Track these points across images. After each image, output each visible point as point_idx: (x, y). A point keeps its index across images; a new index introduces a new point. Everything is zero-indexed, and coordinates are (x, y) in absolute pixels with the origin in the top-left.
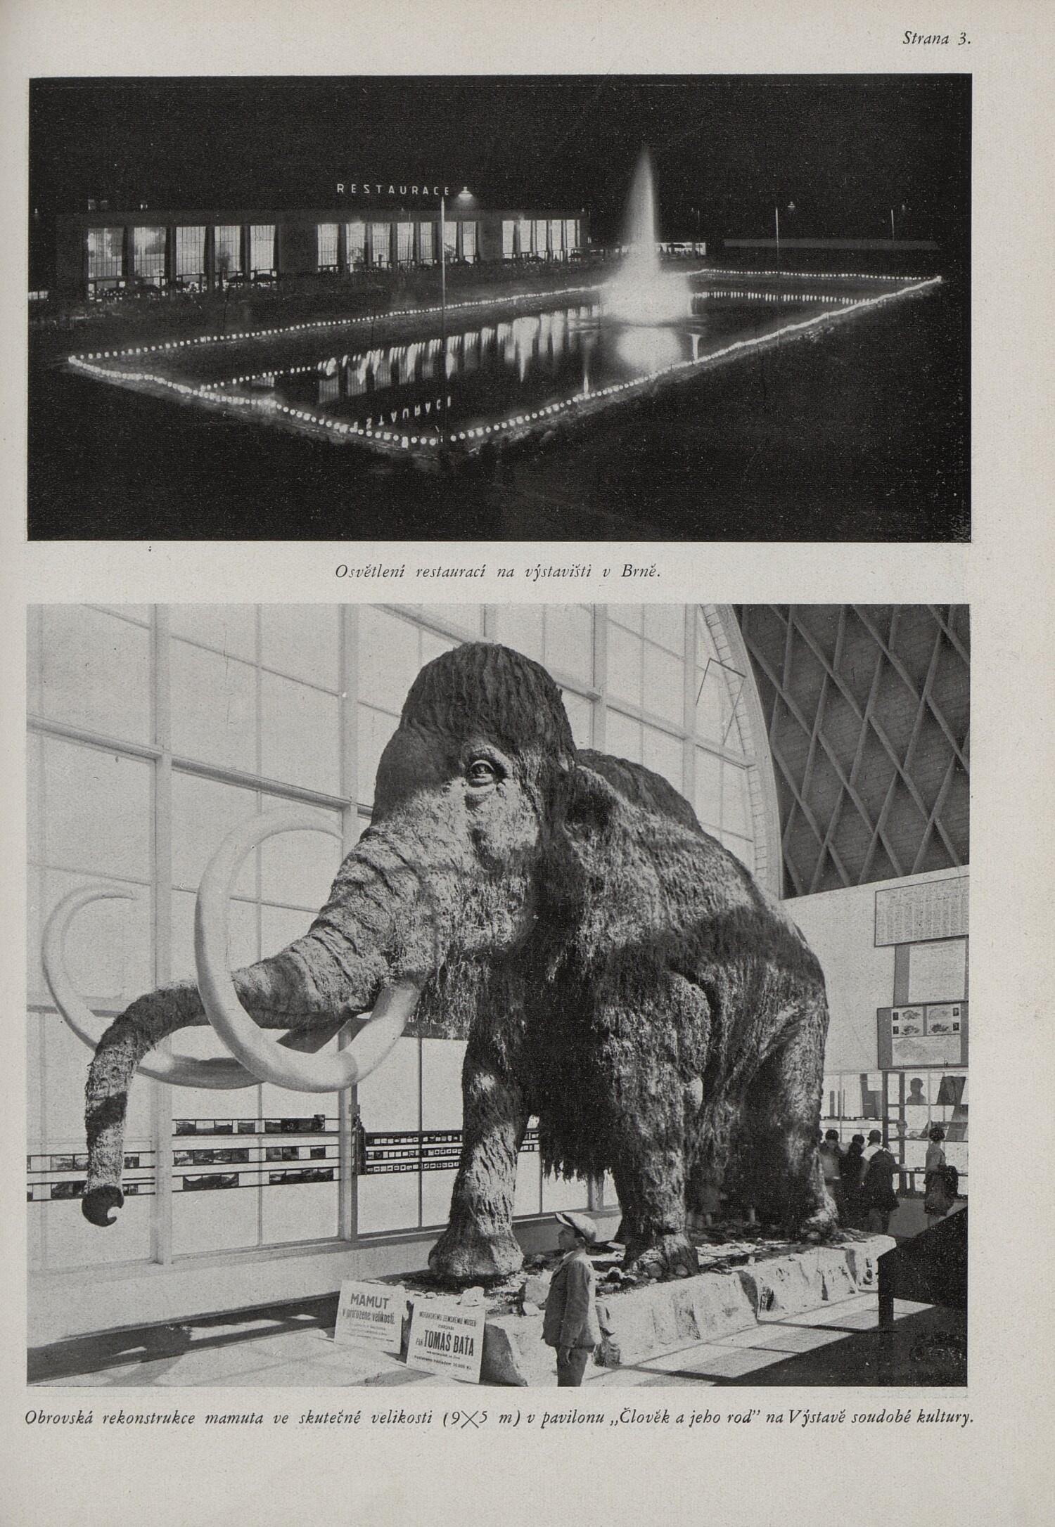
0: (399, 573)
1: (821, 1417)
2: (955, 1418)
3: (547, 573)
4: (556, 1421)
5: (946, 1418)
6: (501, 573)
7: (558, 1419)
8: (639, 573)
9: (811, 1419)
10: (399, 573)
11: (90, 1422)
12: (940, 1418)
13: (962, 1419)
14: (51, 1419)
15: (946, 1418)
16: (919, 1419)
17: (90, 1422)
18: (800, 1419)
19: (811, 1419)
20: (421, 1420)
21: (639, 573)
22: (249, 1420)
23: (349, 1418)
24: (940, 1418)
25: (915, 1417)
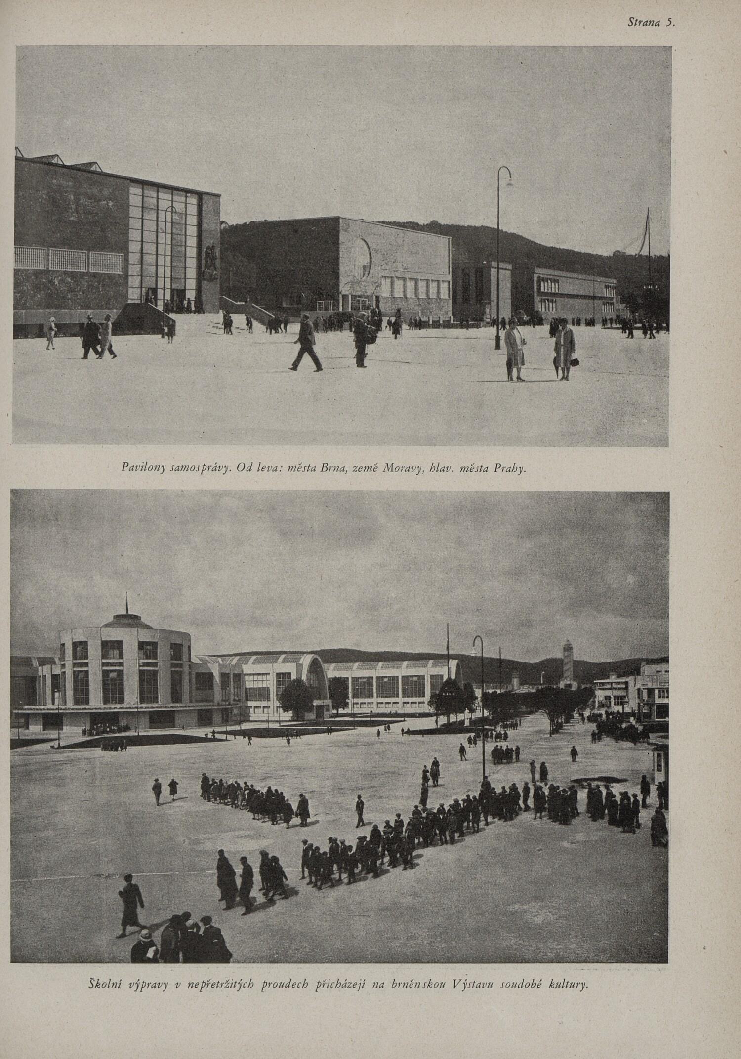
0: (118, 986)
1: (483, 469)
2: (575, 986)
3: (472, 985)
4: (646, 25)
5: (569, 985)
6: (375, 985)
7: (157, 986)
8: (402, 985)
9: (468, 986)
10: (118, 986)
11: (658, 25)
12: (565, 985)
13: (580, 986)
14: (272, 985)
15: (569, 985)
16: (551, 986)
17: (658, 25)
18: (460, 986)
19: (468, 986)
20: (471, 986)
21: (402, 985)
22: (561, 986)
23: (115, 985)
24: (565, 985)
25: (255, 467)
